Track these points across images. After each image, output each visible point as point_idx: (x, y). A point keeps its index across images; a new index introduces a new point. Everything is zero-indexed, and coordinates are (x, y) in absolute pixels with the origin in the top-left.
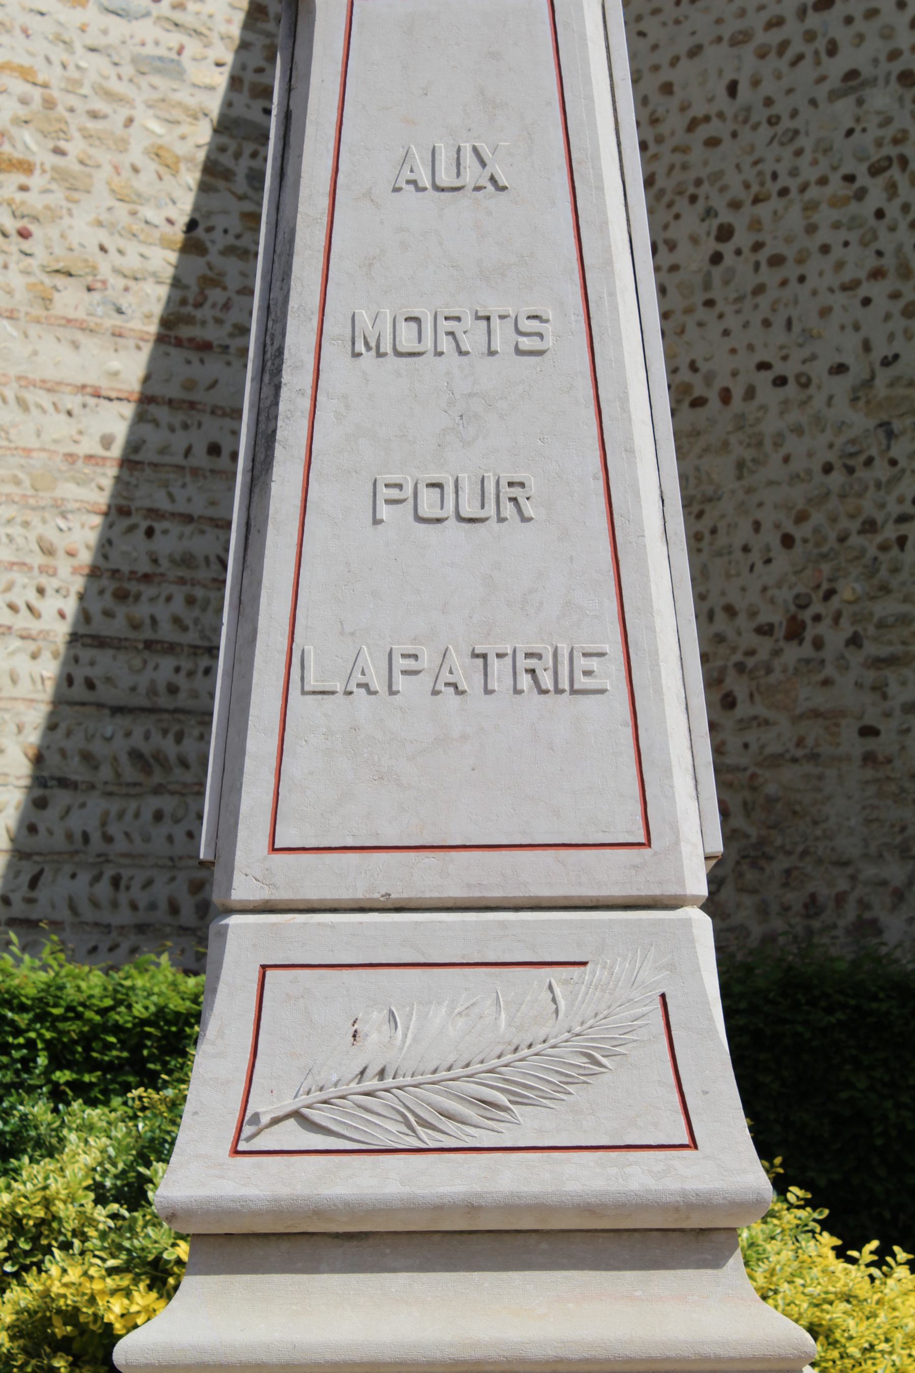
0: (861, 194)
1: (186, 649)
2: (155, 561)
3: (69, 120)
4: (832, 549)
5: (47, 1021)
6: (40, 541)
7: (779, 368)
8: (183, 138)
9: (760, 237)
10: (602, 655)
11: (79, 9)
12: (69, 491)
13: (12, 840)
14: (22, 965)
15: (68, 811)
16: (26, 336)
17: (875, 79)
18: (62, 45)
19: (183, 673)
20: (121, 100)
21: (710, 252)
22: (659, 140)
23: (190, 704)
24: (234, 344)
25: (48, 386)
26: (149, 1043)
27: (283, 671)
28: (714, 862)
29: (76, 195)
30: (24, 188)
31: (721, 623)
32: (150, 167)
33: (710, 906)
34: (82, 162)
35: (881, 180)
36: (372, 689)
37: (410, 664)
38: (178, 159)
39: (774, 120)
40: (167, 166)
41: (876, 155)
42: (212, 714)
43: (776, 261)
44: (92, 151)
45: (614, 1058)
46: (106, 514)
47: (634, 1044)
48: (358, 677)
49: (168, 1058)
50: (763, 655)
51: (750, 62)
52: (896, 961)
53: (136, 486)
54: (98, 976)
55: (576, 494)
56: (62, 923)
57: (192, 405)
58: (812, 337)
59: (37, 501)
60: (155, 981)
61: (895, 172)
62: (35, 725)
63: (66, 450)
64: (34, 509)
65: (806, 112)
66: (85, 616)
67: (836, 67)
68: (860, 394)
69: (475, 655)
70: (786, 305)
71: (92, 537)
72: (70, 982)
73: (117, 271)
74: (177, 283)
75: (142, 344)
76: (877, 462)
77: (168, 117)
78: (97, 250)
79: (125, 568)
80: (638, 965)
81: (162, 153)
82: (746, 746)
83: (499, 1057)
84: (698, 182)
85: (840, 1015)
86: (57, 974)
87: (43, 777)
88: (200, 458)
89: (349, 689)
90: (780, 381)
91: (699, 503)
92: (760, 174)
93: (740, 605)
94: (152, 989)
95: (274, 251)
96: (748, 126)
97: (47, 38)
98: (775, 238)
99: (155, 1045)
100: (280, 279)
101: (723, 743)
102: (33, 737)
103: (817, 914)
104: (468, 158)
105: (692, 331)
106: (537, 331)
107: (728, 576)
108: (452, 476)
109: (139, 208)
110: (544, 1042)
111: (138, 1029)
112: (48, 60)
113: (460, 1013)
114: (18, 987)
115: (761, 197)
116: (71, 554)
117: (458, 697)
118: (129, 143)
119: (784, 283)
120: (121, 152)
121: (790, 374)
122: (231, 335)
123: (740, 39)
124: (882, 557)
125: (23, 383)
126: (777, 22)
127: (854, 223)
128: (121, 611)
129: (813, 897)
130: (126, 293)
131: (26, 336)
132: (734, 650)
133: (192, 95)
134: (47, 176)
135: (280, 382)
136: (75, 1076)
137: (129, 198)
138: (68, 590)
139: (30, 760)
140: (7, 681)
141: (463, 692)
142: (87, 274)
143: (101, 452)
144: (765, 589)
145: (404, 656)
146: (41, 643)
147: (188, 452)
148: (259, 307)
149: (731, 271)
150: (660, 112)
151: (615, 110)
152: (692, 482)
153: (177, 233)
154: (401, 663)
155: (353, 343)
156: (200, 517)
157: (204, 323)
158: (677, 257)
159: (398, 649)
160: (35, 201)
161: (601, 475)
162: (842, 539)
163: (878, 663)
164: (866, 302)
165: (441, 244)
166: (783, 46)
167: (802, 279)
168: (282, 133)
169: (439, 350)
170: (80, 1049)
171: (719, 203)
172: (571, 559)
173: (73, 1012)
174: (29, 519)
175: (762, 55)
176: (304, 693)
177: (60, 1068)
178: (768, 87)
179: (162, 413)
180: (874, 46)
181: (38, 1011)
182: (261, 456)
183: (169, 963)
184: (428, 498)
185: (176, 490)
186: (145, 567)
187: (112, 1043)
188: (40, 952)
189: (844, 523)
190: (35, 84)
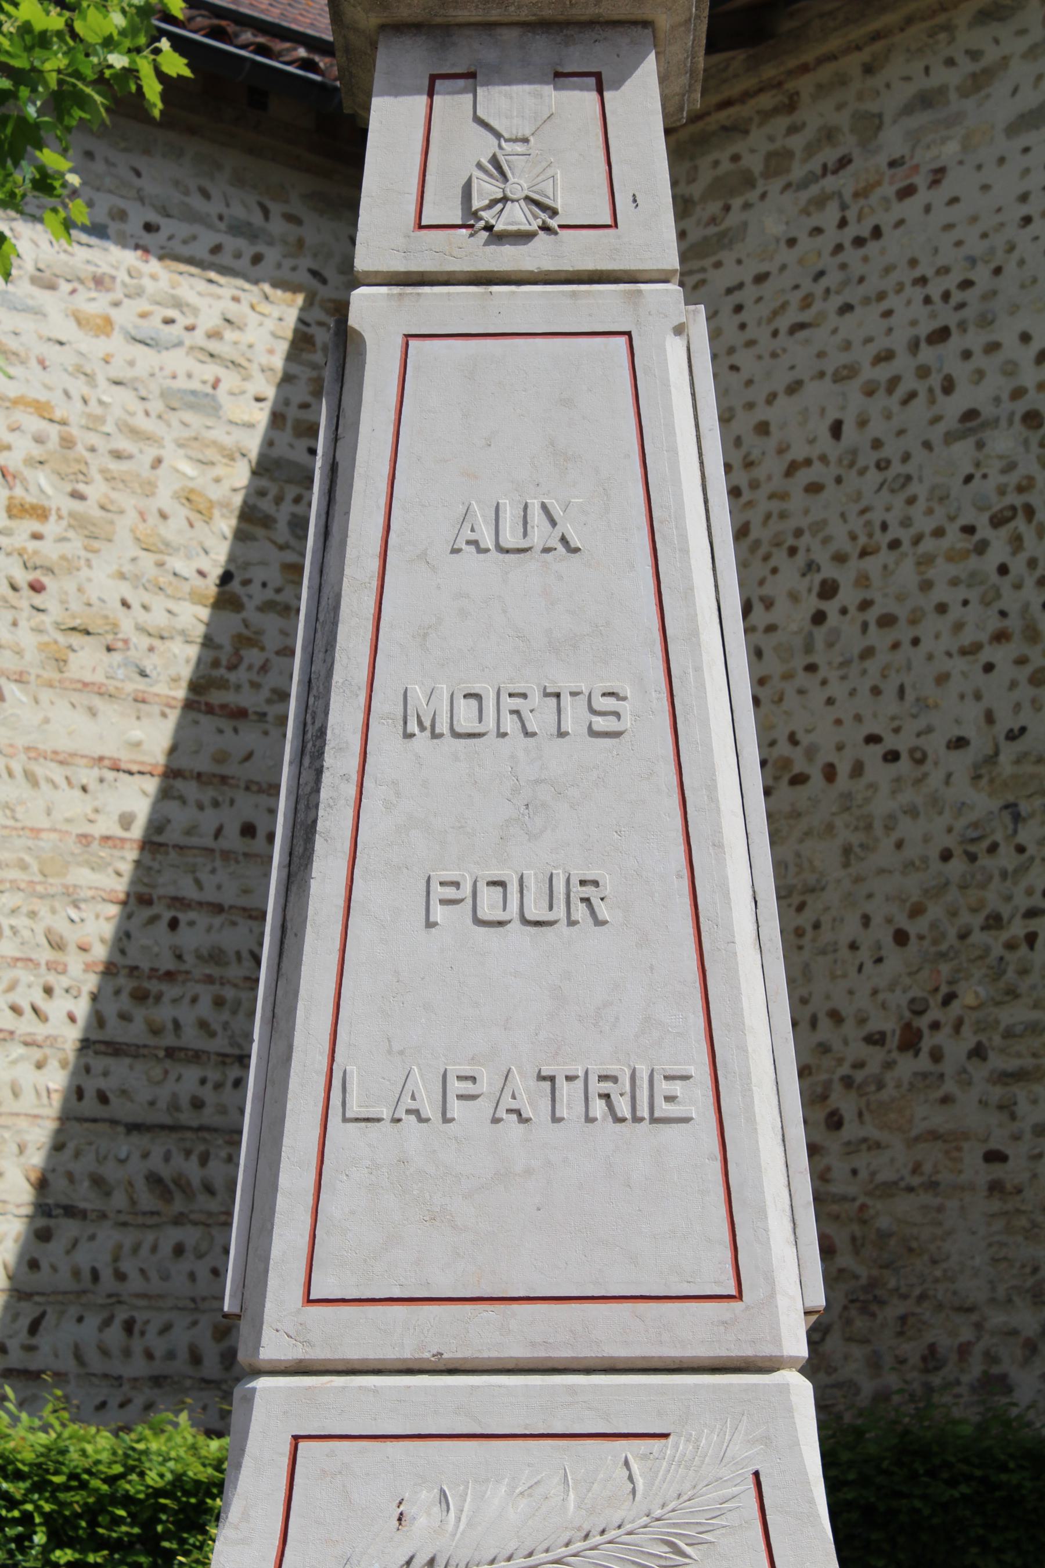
0: (981, 548)
1: (213, 1057)
2: (179, 957)
3: (90, 461)
4: (951, 947)
5: (46, 1491)
6: (48, 934)
7: (890, 742)
8: (217, 480)
9: (868, 595)
10: (686, 1078)
11: (103, 338)
12: (83, 877)
13: (10, 1278)
14: (19, 1424)
15: (75, 1243)
16: (37, 701)
17: (997, 420)
18: (82, 377)
19: (209, 1085)
20: (148, 439)
21: (812, 611)
22: (754, 485)
23: (217, 1121)
24: (272, 711)
25: (61, 757)
26: (164, 1517)
27: (322, 1095)
28: (814, 1318)
29: (96, 544)
30: (37, 536)
31: (826, 1031)
32: (180, 513)
33: (810, 1369)
34: (103, 508)
35: (1005, 531)
36: (423, 1116)
37: (467, 1087)
38: (211, 504)
39: (883, 465)
40: (200, 512)
41: (998, 504)
42: (240, 1132)
43: (887, 621)
44: (114, 495)
45: (700, 1547)
46: (124, 903)
47: (723, 1531)
48: (407, 1102)
49: (185, 1535)
50: (873, 1067)
51: (856, 400)
52: (1029, 1424)
53: (159, 871)
54: (106, 1438)
55: (657, 895)
56: (66, 1374)
57: (224, 779)
58: (927, 706)
59: (46, 889)
60: (173, 1444)
61: (1020, 523)
62: (39, 1145)
63: (80, 831)
64: (41, 897)
65: (919, 455)
66: (98, 1019)
67: (953, 407)
68: (983, 771)
69: (541, 1078)
70: (898, 671)
71: (108, 930)
72: (73, 1444)
73: (141, 629)
74: (208, 642)
75: (168, 711)
76: (1002, 850)
77: (201, 457)
78: (119, 605)
79: (145, 965)
80: (727, 1437)
81: (193, 497)
82: (854, 1172)
83: (567, 1545)
84: (798, 533)
85: (964, 1489)
86: (59, 1436)
87: (47, 1205)
88: (232, 840)
89: (396, 1116)
90: (892, 756)
91: (797, 895)
92: (868, 523)
93: (847, 1010)
94: (168, 1453)
95: (317, 619)
96: (853, 472)
97: (66, 370)
98: (886, 595)
99: (171, 1519)
100: (323, 650)
101: (828, 1169)
102: (37, 1159)
103: (937, 1369)
104: (536, 515)
105: (792, 700)
106: (613, 709)
107: (833, 977)
108: (516, 872)
109: (167, 558)
110: (619, 1527)
111: (152, 1501)
112: (67, 394)
113: (521, 1493)
114: (14, 1451)
115: (869, 550)
116: (83, 949)
117: (522, 1125)
118: (156, 487)
119: (896, 646)
120: (147, 496)
121: (903, 749)
122: (269, 701)
123: (845, 374)
124: (1009, 956)
125: (33, 754)
126: (886, 356)
127: (974, 579)
128: (139, 1014)
129: (932, 1348)
130: (151, 654)
131: (37, 701)
132: (840, 1061)
133: (228, 433)
134: (64, 523)
135: (322, 766)
136: (77, 1556)
137: (156, 548)
138: (79, 991)
139: (32, 1184)
140: (8, 1093)
141: (528, 1120)
142: (107, 632)
143: (120, 833)
144: (875, 992)
145: (460, 1078)
146: (47, 1051)
147: (218, 833)
148: (299, 682)
149: (836, 632)
150: (755, 454)
151: (702, 463)
152: (792, 869)
153: (210, 587)
154: (456, 1087)
155: (405, 723)
156: (231, 907)
157: (238, 687)
158: (775, 616)
159: (454, 1070)
160: (49, 550)
161: (685, 873)
162: (963, 936)
163: (1006, 1078)
164: (989, 668)
165: (505, 612)
166: (894, 382)
167: (916, 642)
168: (327, 487)
169: (502, 731)
170: (83, 1524)
171: (822, 556)
172: (652, 968)
173: (77, 1480)
174: (36, 908)
175: (870, 393)
176: (345, 1120)
177: (61, 1546)
178: (877, 428)
179: (190, 789)
180: (996, 383)
181: (36, 1479)
182: (299, 850)
183: (189, 1423)
184: (489, 899)
185: (204, 876)
186: (167, 964)
187: (121, 1517)
188: (41, 1409)
189: (965, 918)
190: (51, 420)
